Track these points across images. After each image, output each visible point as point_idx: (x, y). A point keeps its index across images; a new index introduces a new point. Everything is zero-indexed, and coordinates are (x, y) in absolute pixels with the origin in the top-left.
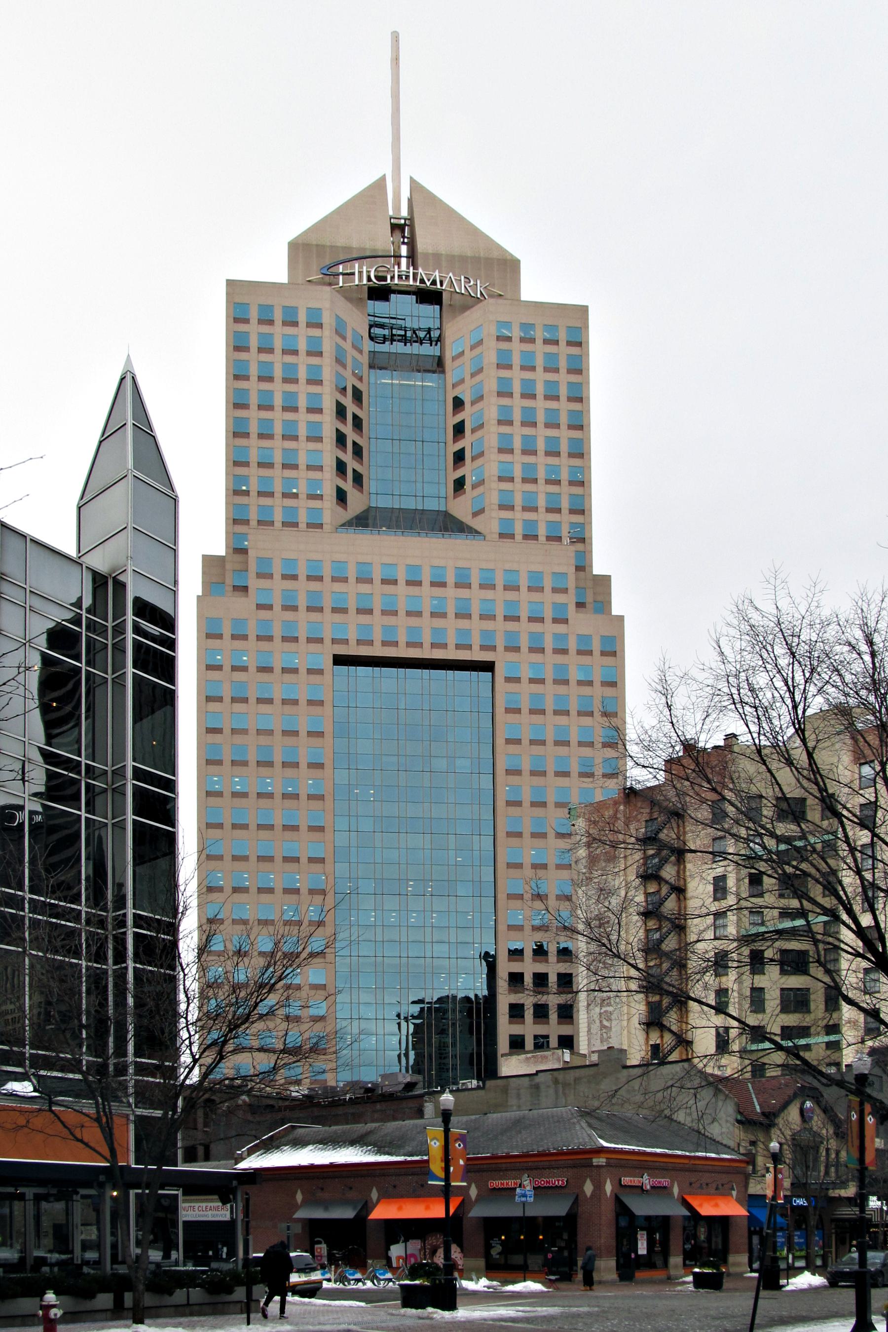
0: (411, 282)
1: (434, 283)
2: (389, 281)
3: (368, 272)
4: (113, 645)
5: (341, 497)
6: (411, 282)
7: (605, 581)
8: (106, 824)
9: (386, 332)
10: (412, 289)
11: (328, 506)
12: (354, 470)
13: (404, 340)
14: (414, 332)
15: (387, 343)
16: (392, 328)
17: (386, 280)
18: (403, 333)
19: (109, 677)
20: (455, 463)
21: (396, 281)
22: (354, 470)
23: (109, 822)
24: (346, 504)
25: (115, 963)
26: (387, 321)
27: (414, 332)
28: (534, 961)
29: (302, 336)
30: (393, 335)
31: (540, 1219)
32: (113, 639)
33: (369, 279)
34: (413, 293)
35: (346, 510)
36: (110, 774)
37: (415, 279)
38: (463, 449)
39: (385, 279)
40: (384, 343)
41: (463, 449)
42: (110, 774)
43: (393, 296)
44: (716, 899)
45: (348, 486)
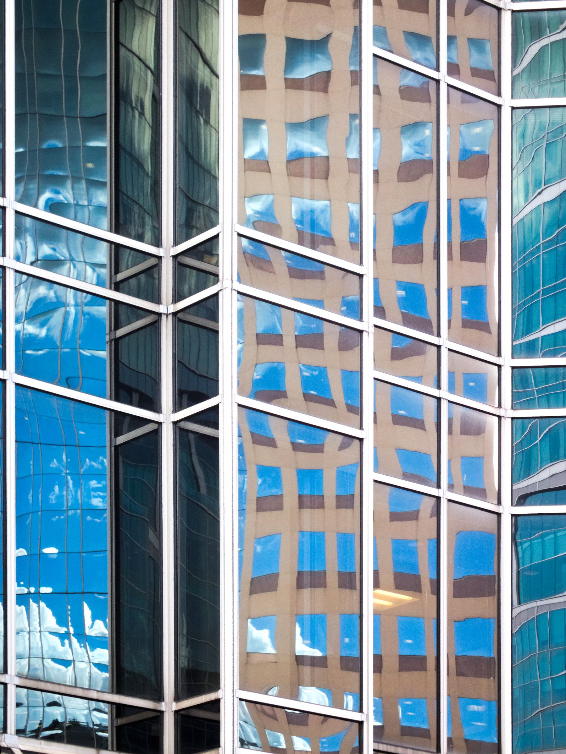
43: (23, 607)
44: (280, 507)
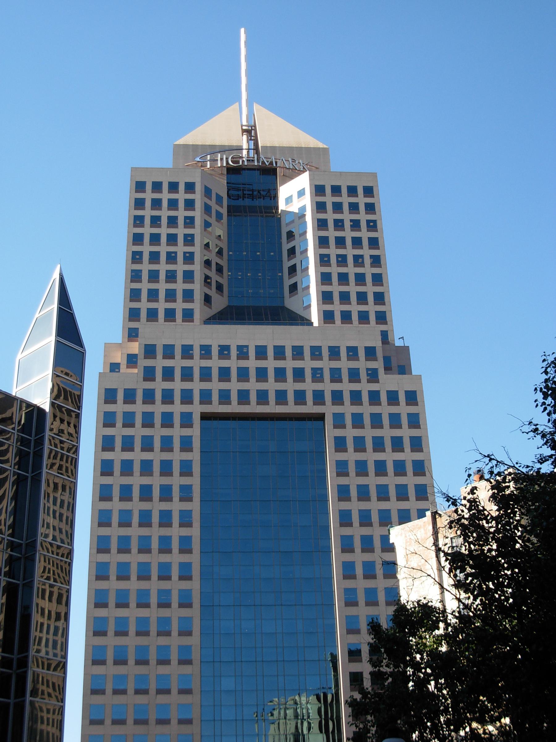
0: (256, 164)
1: (271, 163)
2: (241, 163)
3: (227, 159)
4: (34, 453)
5: (207, 299)
6: (256, 164)
7: (405, 350)
8: (21, 544)
9: (240, 193)
10: (256, 167)
11: (197, 306)
12: (217, 264)
13: (252, 197)
14: (259, 192)
15: (241, 200)
16: (243, 190)
17: (239, 163)
18: (251, 193)
19: (29, 475)
20: (291, 292)
21: (246, 164)
22: (217, 264)
23: (29, 475)
24: (211, 304)
25: (16, 698)
26: (241, 186)
27: (259, 192)
28: (353, 248)
29: (181, 196)
30: (244, 194)
31: (369, 377)
32: (34, 449)
33: (227, 163)
34: (258, 170)
35: (211, 308)
36: (24, 546)
37: (258, 161)
38: (295, 265)
39: (238, 162)
40: (238, 199)
41: (295, 265)
42: (24, 546)
45: (212, 292)
